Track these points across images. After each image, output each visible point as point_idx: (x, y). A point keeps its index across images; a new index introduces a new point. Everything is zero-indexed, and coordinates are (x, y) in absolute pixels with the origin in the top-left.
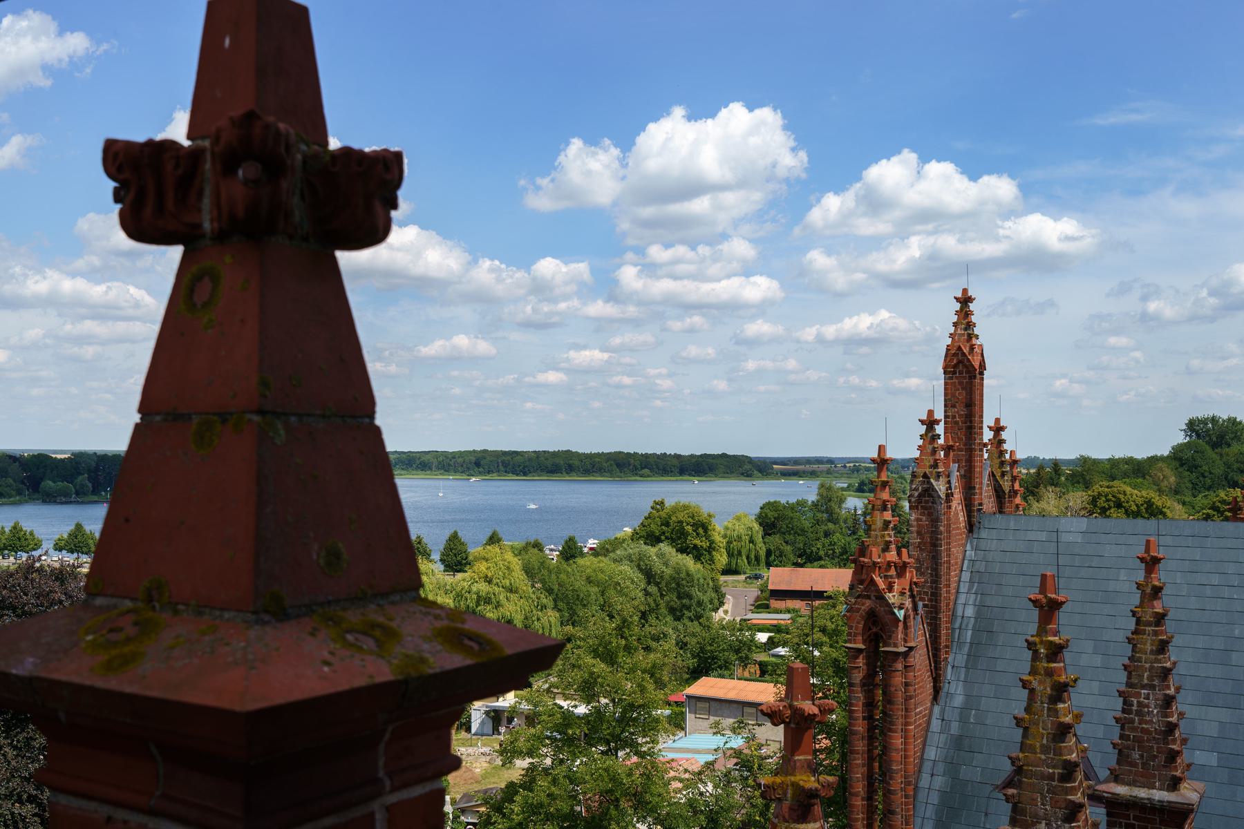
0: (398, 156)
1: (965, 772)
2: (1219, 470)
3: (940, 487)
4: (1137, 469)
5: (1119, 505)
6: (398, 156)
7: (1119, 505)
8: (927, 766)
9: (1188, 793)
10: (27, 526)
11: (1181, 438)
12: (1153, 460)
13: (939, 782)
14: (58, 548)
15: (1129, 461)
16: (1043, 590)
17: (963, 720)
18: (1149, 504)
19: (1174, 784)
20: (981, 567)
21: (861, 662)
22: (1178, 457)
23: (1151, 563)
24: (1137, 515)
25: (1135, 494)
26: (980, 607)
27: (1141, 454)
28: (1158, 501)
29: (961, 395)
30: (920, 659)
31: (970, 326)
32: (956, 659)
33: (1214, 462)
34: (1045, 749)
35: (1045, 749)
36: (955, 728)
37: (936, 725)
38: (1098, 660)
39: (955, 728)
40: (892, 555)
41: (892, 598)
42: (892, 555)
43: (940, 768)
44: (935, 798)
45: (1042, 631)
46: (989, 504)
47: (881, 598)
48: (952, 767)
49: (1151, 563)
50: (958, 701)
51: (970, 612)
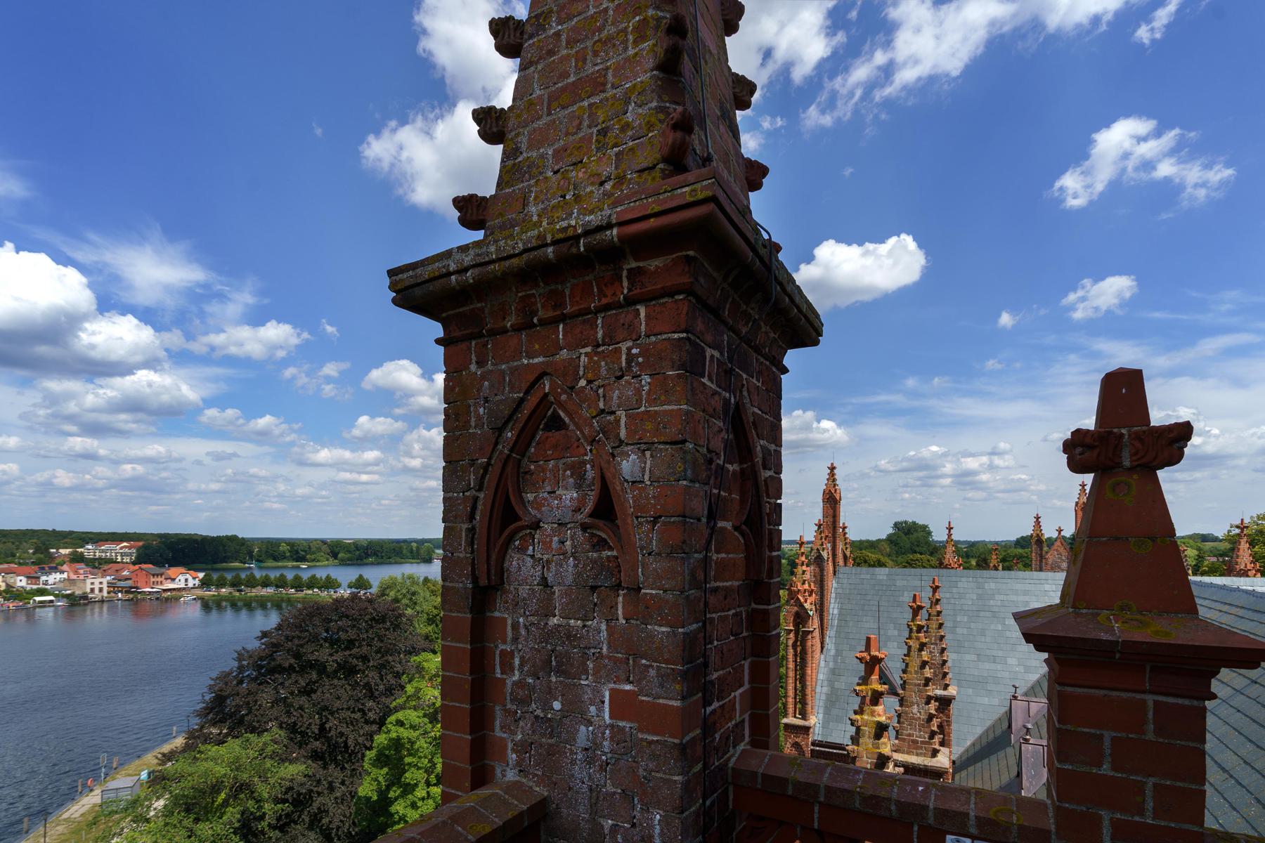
0: (1138, 373)
1: (837, 685)
2: (908, 546)
3: (825, 554)
4: (872, 545)
5: (865, 562)
6: (1138, 373)
7: (865, 562)
8: (819, 683)
9: (952, 691)
10: (333, 576)
11: (891, 531)
12: (879, 541)
13: (825, 690)
14: (350, 587)
15: (868, 541)
16: (914, 601)
17: (835, 661)
18: (879, 561)
19: (946, 687)
20: (840, 591)
21: (792, 635)
22: (890, 540)
23: (935, 589)
24: (874, 566)
25: (873, 556)
26: (841, 609)
27: (874, 538)
28: (883, 559)
29: (831, 512)
30: (817, 634)
31: (834, 480)
32: (830, 633)
33: (905, 541)
34: (916, 672)
35: (916, 672)
36: (831, 665)
37: (822, 664)
38: (896, 633)
39: (831, 665)
40: (806, 586)
41: (807, 606)
42: (806, 586)
43: (825, 683)
44: (823, 697)
45: (913, 620)
46: (841, 562)
47: (802, 606)
48: (831, 683)
49: (935, 589)
50: (833, 652)
51: (836, 612)
